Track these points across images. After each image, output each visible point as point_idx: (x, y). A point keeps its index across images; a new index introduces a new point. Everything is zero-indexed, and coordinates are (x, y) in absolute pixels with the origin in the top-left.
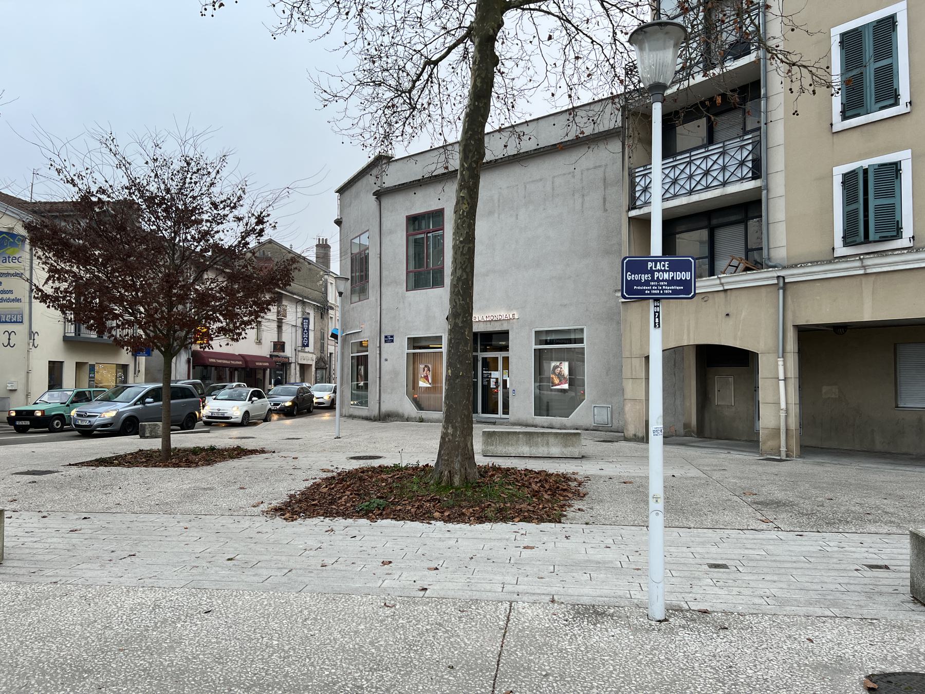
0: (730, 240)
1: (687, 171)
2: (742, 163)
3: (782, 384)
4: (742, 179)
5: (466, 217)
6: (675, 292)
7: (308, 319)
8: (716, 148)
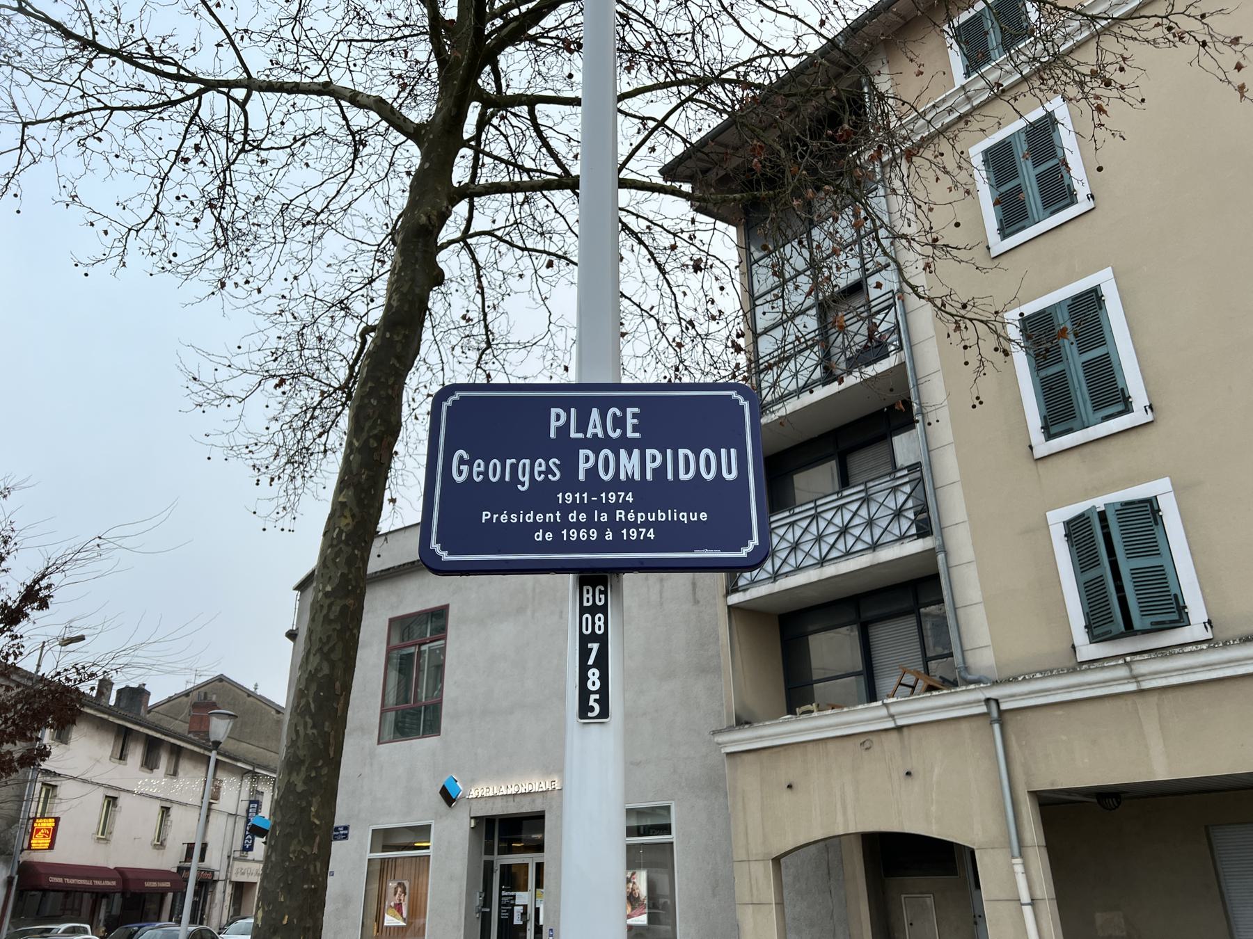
0: (896, 641)
1: (813, 529)
2: (898, 514)
3: (1028, 911)
4: (902, 538)
5: (346, 542)
6: (670, 536)
7: (258, 802)
8: (853, 492)
